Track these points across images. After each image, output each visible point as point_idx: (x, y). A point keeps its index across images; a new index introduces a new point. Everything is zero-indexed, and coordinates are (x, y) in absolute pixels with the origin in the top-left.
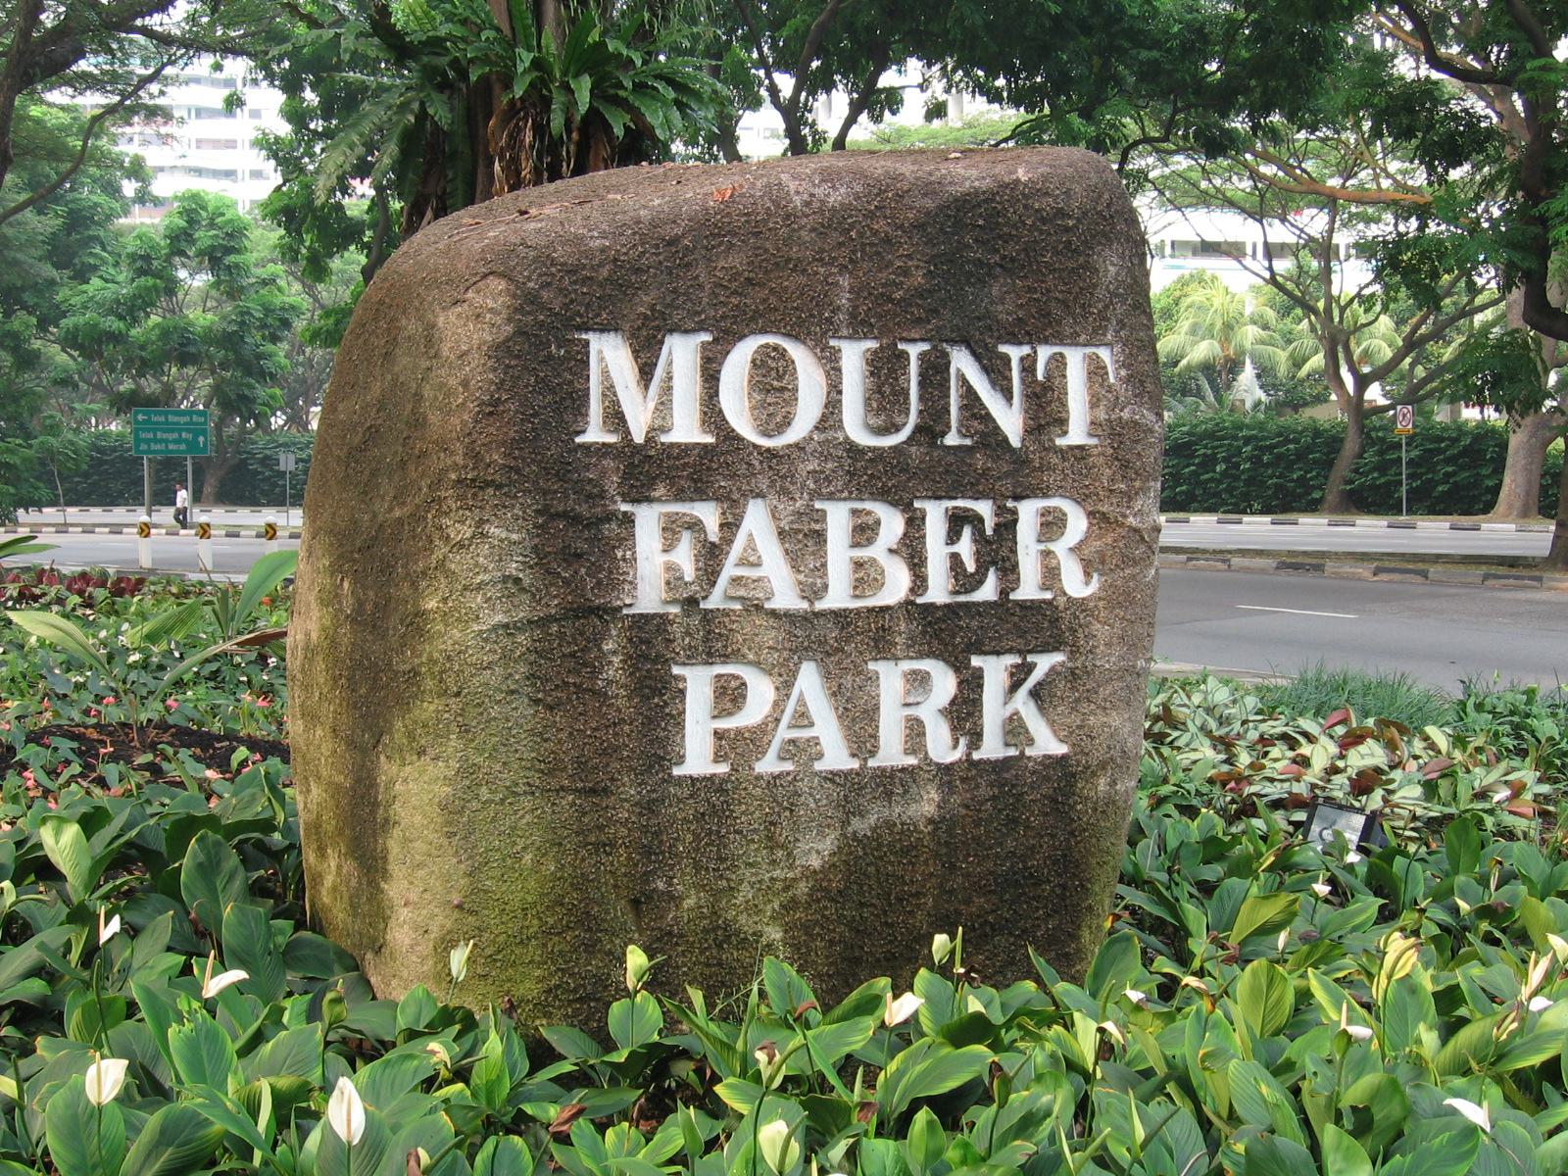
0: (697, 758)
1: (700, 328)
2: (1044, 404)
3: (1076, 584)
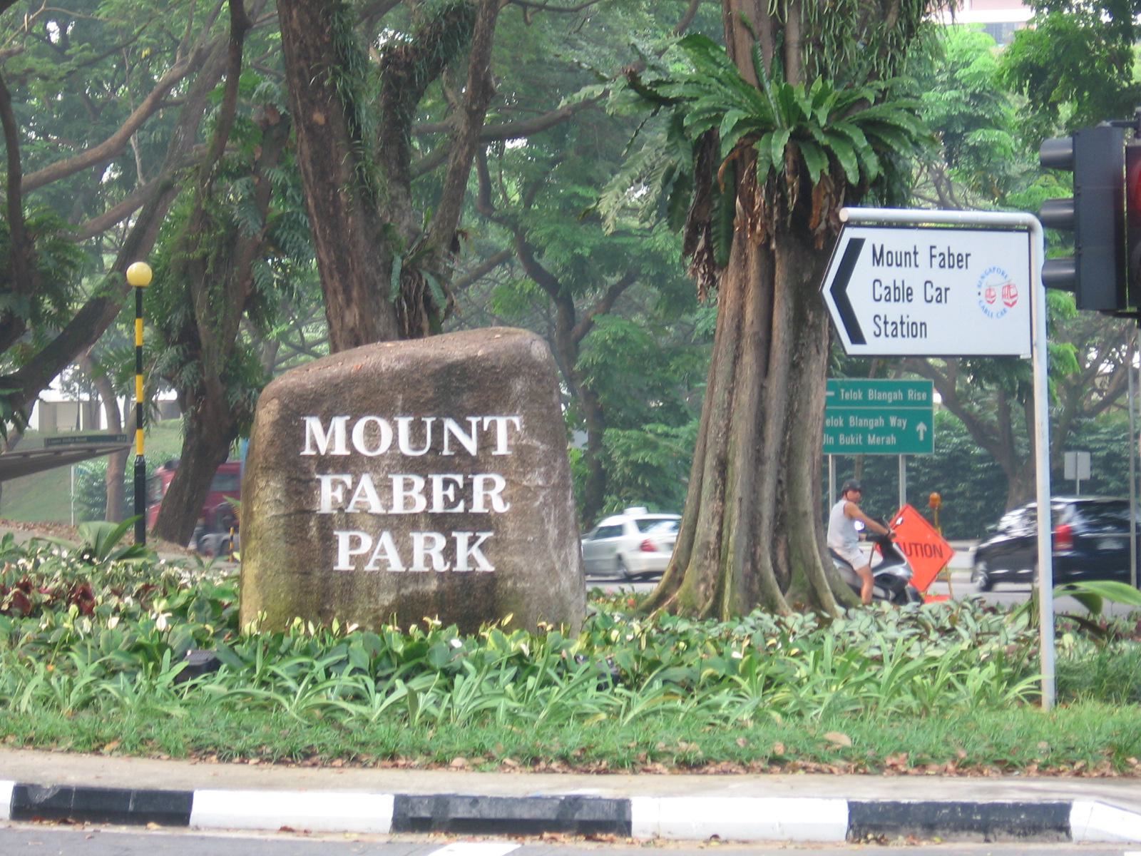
0: (343, 562)
1: (345, 414)
2: (487, 440)
3: (499, 507)
